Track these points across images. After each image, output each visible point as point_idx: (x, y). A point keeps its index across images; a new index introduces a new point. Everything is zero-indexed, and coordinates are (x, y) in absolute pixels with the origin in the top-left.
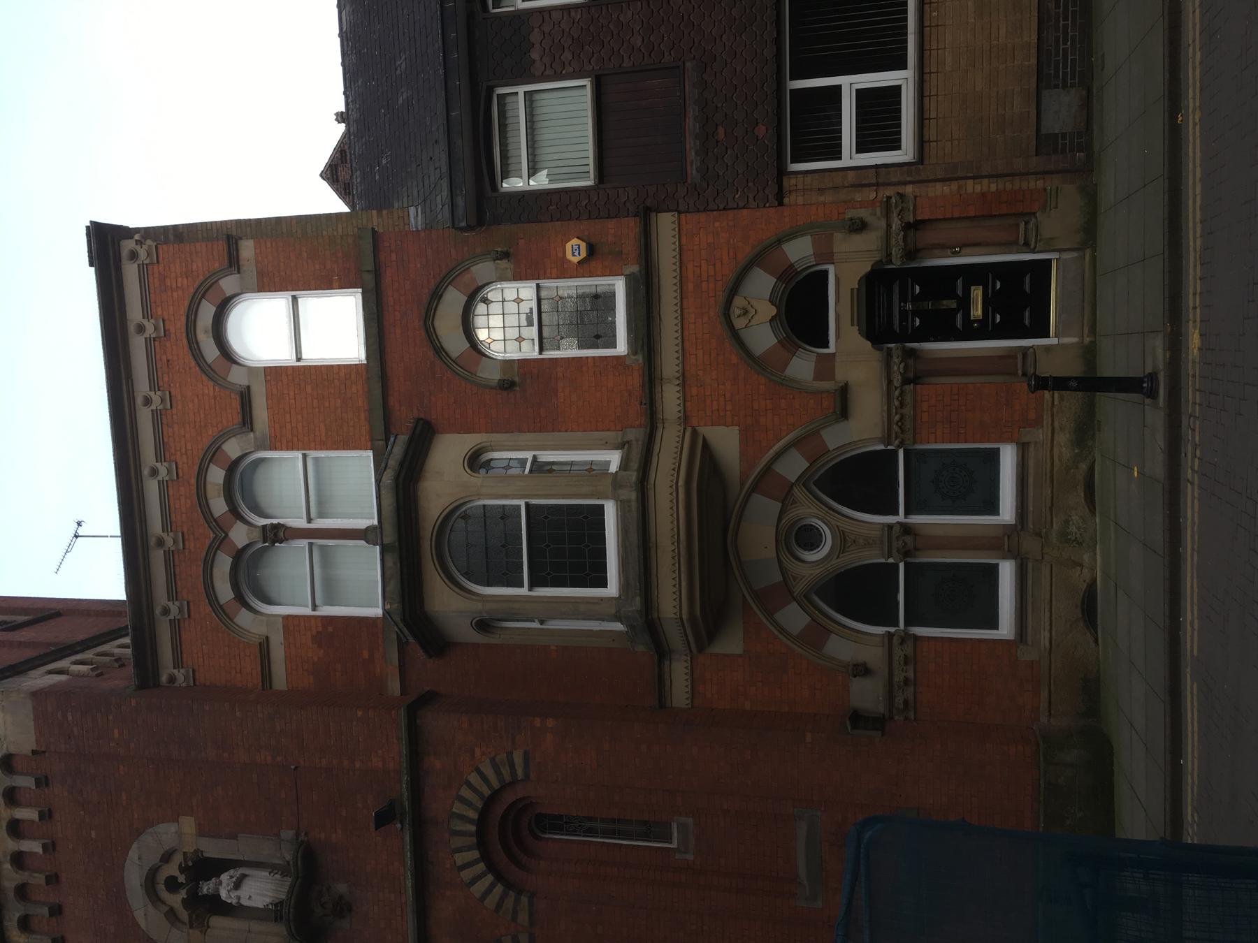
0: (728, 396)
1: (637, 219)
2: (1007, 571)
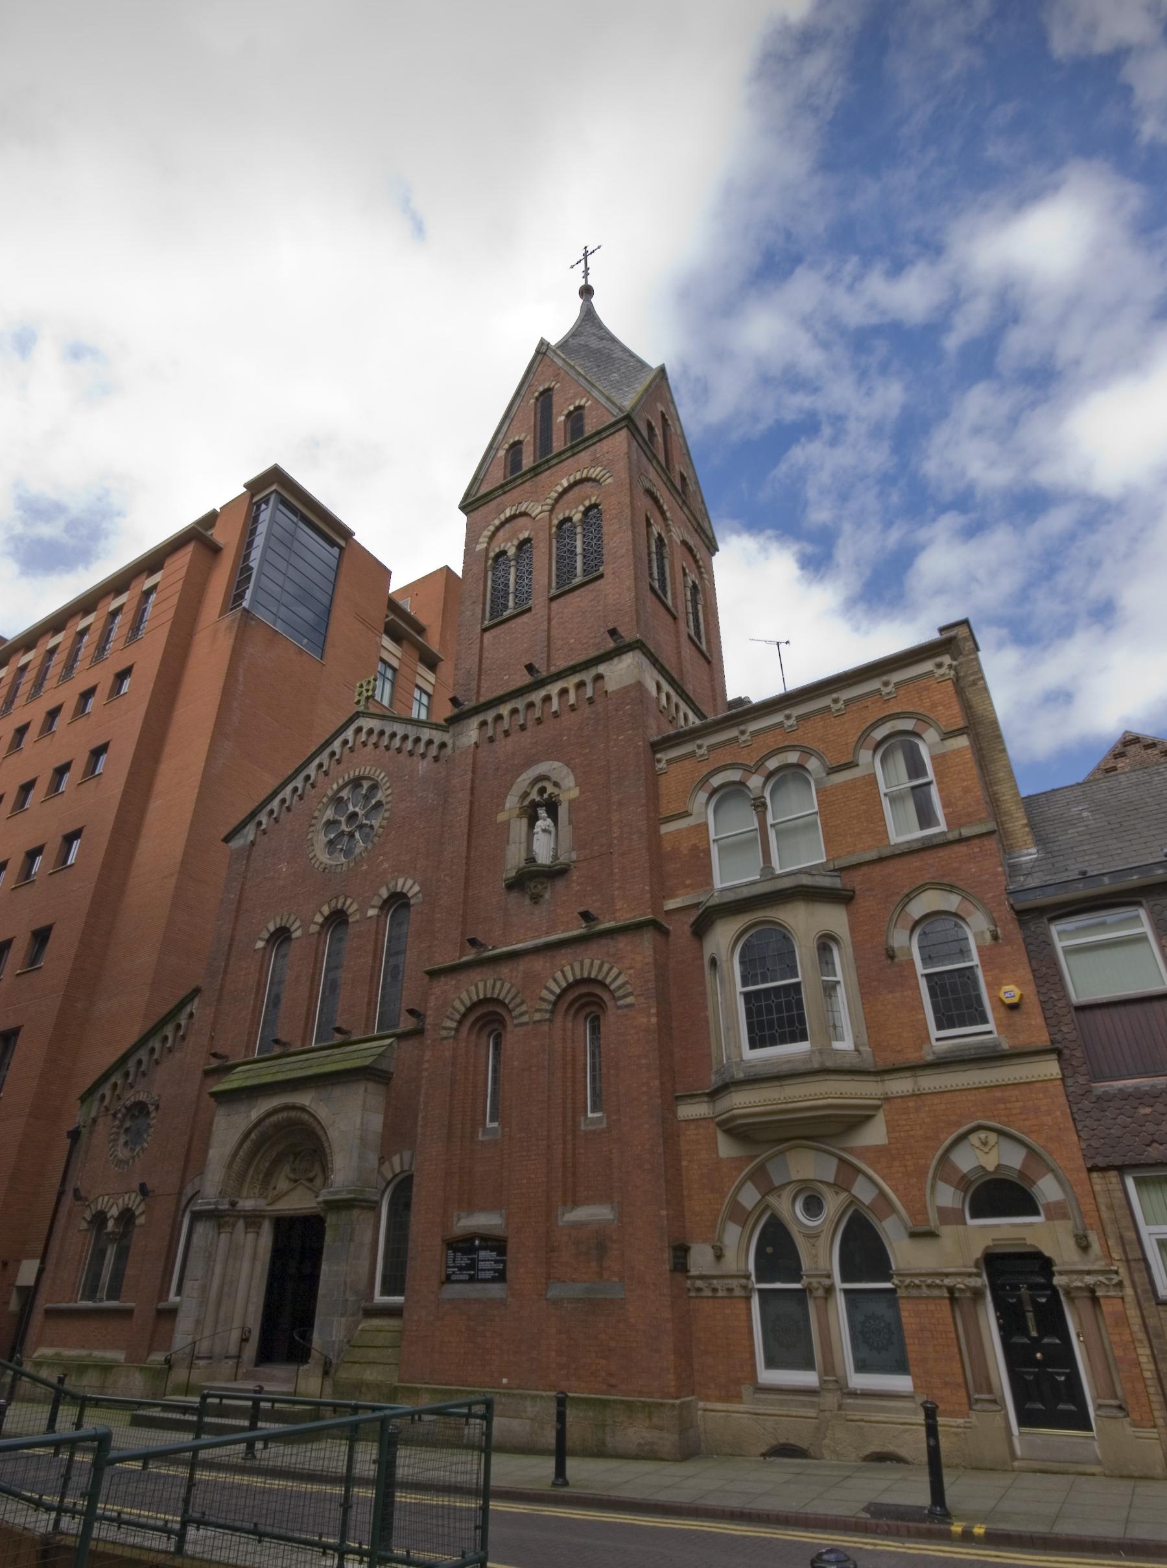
0: (912, 1133)
1: (1049, 1043)
2: (808, 1378)
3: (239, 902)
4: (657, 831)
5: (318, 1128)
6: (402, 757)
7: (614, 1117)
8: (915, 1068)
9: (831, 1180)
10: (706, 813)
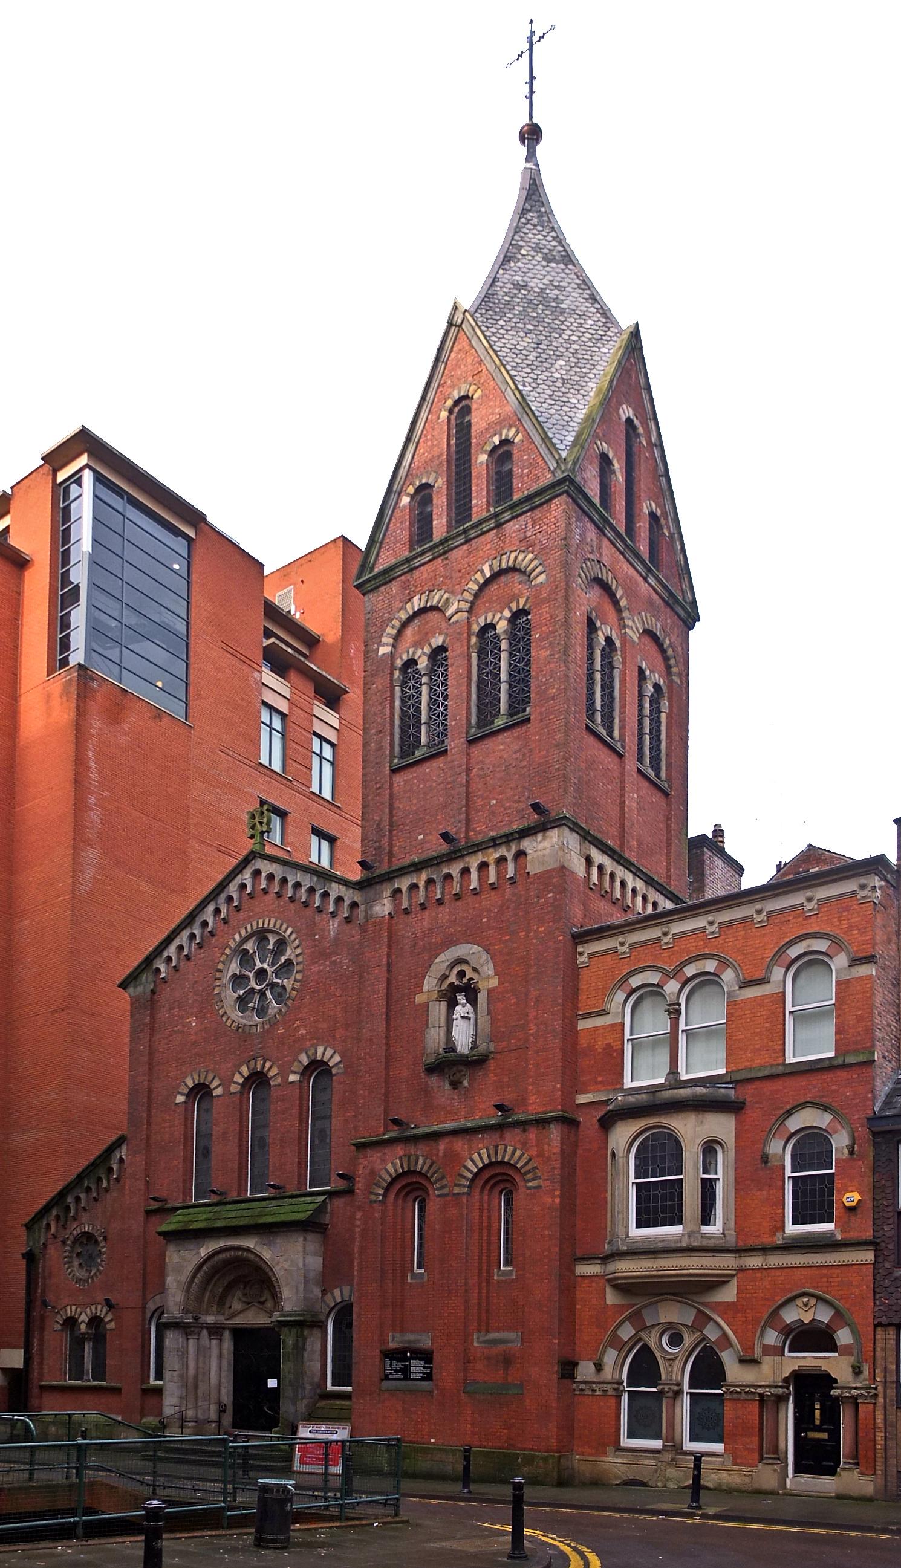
2: (657, 1444)
3: (150, 1054)
6: (308, 912)
7: (521, 1272)
8: (765, 1250)
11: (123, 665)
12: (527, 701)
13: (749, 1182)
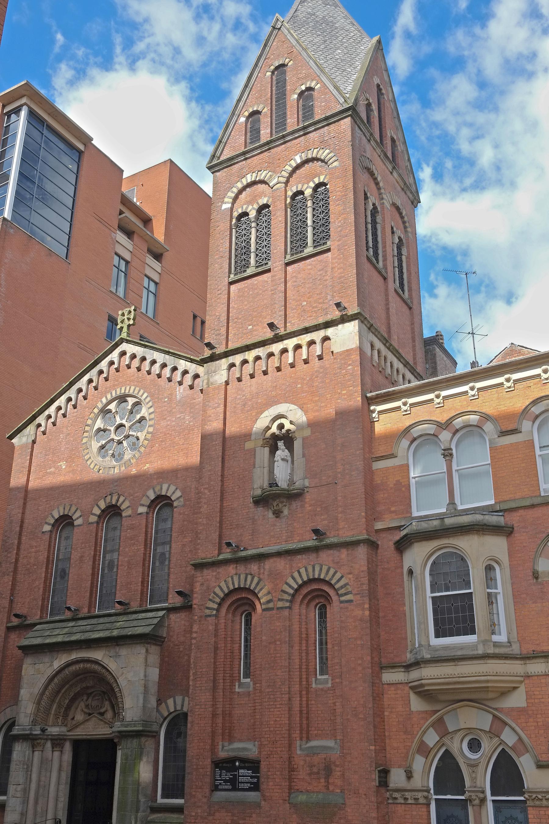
0: (543, 700)
4: (371, 467)
5: (109, 677)
7: (337, 680)
9: (488, 730)
10: (408, 456)
11: (32, 221)
12: (327, 237)
13: (524, 596)
